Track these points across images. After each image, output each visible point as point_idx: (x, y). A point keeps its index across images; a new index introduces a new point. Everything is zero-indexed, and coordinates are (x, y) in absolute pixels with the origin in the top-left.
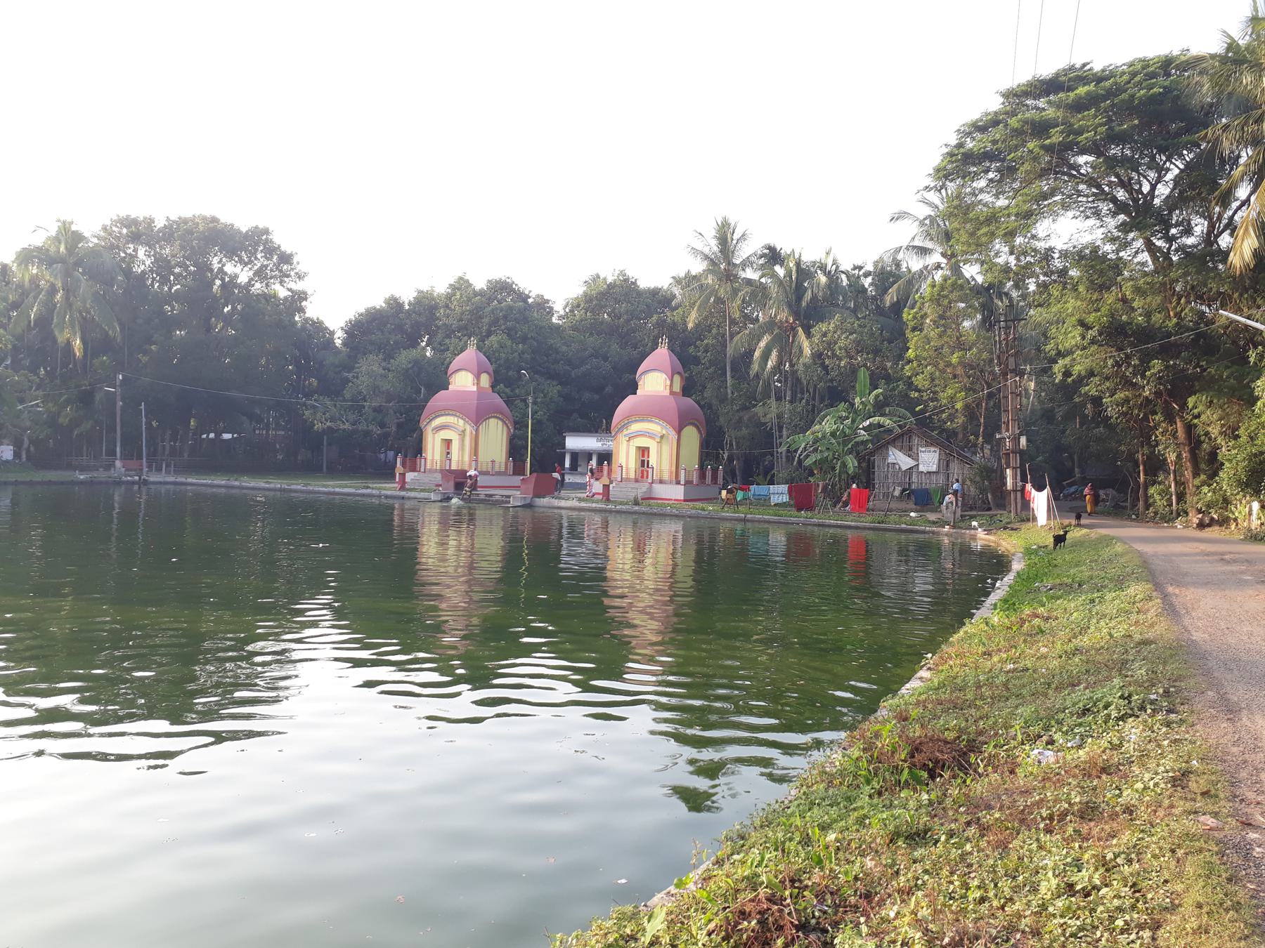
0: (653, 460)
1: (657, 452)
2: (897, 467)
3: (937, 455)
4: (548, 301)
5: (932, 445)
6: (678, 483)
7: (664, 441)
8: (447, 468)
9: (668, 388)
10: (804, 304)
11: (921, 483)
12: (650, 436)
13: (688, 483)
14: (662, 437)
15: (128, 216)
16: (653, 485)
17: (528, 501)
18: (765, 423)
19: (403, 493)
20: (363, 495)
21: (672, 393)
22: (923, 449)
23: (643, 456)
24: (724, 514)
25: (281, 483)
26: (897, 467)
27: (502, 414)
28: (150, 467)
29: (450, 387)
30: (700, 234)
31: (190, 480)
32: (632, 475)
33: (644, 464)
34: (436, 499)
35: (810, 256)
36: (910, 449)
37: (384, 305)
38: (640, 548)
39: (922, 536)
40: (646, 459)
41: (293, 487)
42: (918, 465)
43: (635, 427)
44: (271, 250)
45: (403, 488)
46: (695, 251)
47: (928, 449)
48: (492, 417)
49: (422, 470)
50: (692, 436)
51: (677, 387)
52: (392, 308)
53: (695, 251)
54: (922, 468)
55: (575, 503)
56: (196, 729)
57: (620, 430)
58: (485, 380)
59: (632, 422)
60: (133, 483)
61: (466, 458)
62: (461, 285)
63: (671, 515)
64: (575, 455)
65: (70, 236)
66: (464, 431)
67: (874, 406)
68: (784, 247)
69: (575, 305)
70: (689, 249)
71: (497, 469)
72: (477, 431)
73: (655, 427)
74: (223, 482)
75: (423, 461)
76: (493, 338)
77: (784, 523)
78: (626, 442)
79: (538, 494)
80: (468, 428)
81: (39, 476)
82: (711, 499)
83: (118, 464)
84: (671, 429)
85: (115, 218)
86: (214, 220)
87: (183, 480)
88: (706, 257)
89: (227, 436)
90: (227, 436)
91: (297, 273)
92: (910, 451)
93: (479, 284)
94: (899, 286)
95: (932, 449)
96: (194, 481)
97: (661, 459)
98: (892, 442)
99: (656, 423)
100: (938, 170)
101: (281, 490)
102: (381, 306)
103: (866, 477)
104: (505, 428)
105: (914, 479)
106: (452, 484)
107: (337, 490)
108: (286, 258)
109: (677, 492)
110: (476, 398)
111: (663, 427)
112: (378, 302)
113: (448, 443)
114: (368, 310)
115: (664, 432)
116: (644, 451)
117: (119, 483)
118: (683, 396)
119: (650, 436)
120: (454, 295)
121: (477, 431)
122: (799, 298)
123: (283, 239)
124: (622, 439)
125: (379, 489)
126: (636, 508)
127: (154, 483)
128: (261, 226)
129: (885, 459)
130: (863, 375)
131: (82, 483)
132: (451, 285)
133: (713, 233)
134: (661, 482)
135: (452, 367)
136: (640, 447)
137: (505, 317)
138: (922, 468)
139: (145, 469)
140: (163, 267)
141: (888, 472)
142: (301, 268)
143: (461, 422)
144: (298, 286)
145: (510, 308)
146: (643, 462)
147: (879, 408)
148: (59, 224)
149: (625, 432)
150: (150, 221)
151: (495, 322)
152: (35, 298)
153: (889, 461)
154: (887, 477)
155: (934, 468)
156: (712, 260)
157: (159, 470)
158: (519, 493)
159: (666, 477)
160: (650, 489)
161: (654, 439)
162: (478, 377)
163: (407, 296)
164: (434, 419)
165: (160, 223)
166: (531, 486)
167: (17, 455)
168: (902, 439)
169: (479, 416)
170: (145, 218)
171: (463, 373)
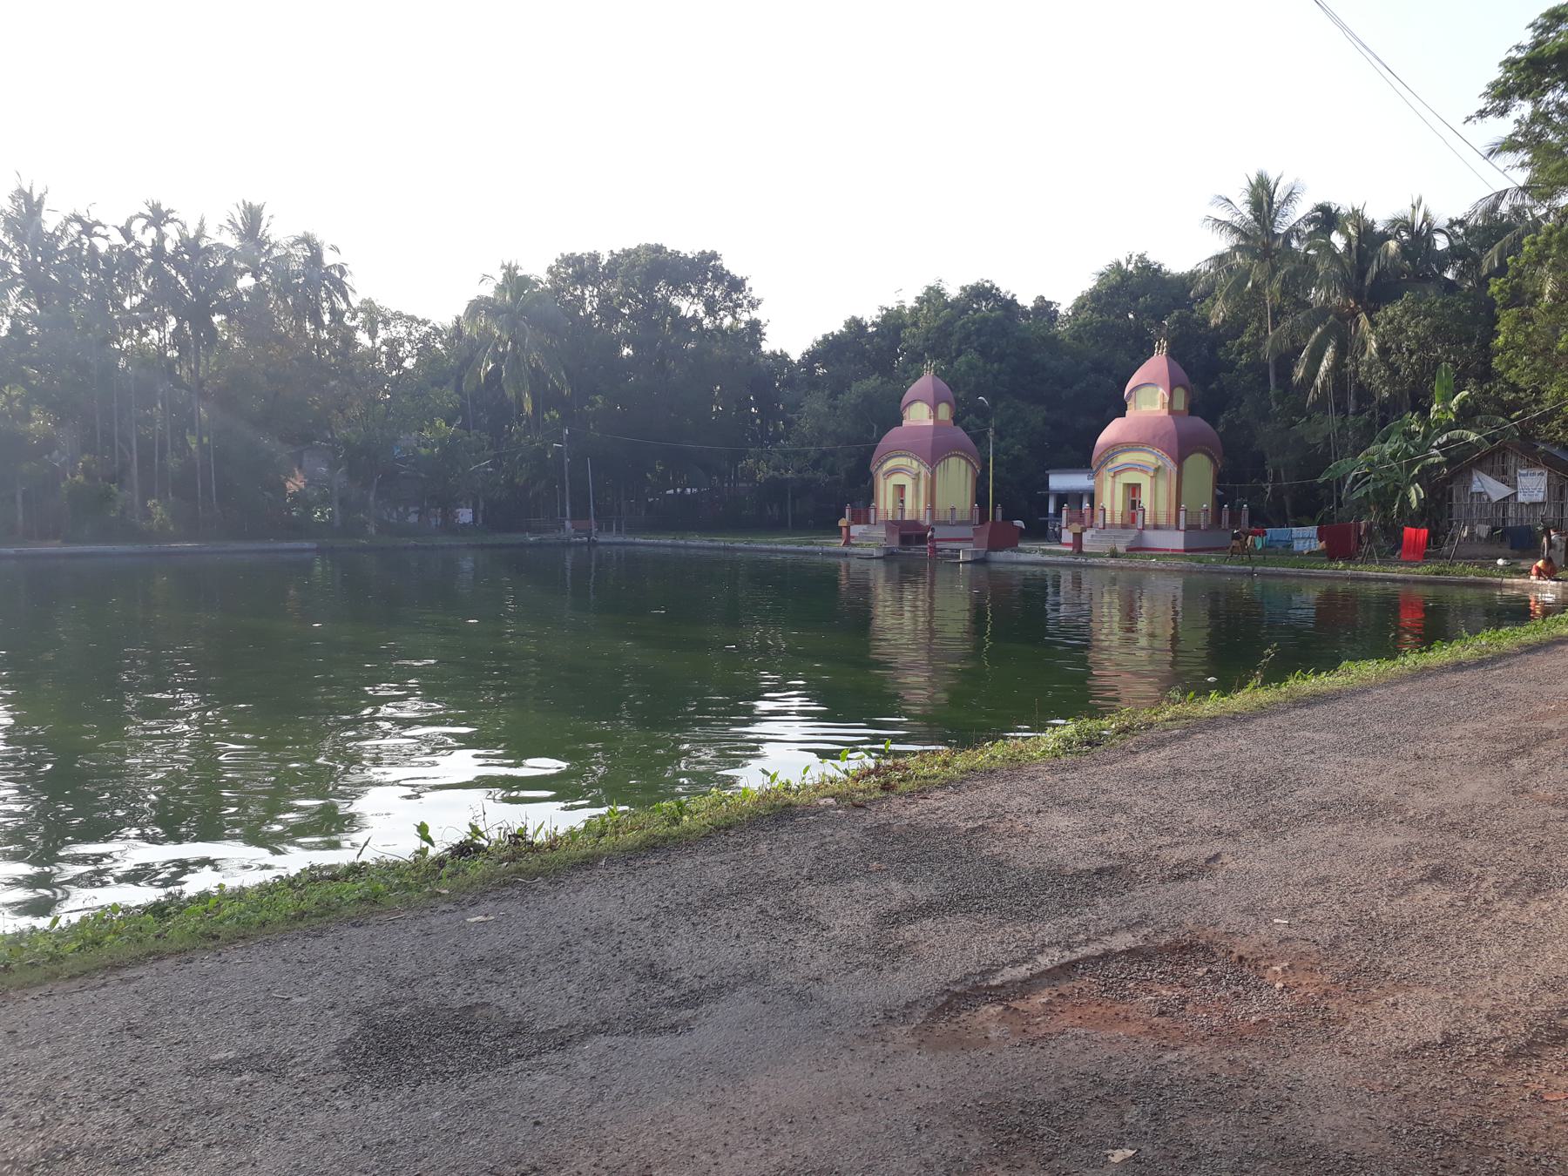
0: (1145, 499)
1: (1151, 489)
2: (1486, 497)
3: (1544, 479)
4: (1051, 303)
5: (1537, 465)
6: (1178, 528)
7: (1159, 475)
8: (899, 518)
9: (1166, 406)
10: (1368, 282)
11: (1521, 519)
12: (1142, 468)
13: (1188, 528)
14: (1157, 470)
15: (573, 254)
16: (1145, 532)
17: (981, 555)
18: (1314, 445)
19: (1081, 560)
20: (806, 553)
21: (1171, 412)
22: (1524, 472)
23: (1134, 495)
24: (1224, 567)
25: (725, 541)
26: (1486, 497)
27: (965, 451)
28: (600, 529)
29: (904, 422)
30: (1228, 200)
31: (637, 540)
32: (1118, 520)
33: (1134, 505)
34: (879, 555)
35: (1379, 215)
36: (1505, 472)
37: (844, 330)
38: (1130, 615)
39: (632, 548)
40: (1137, 498)
41: (737, 545)
42: (1515, 494)
43: (1123, 459)
44: (721, 276)
45: (847, 543)
46: (1220, 224)
47: (1531, 471)
48: (952, 456)
49: (873, 522)
50: (1201, 468)
51: (1180, 404)
52: (852, 333)
53: (1220, 224)
54: (1521, 498)
55: (1038, 557)
56: (519, 775)
57: (1104, 463)
58: (944, 412)
59: (1117, 453)
60: (582, 544)
61: (922, 507)
62: (933, 296)
63: (1156, 570)
64: (1063, 498)
65: (514, 282)
66: (918, 475)
67: (1457, 415)
68: (1343, 202)
69: (1080, 306)
70: (1211, 223)
71: (958, 518)
72: (933, 474)
73: (1148, 458)
74: (669, 541)
75: (872, 511)
76: (962, 359)
77: (1306, 577)
78: (1110, 479)
79: (995, 545)
80: (923, 470)
81: (499, 538)
82: (1221, 548)
83: (568, 524)
84: (1169, 459)
85: (560, 258)
86: (659, 249)
87: (631, 540)
88: (1235, 230)
89: (671, 492)
90: (671, 492)
91: (749, 302)
92: (1504, 476)
93: (953, 292)
94: (1502, 246)
95: (1538, 471)
96: (642, 541)
97: (1156, 499)
98: (1480, 464)
99: (1150, 452)
100: (1494, 86)
101: (726, 549)
102: (841, 331)
103: (1437, 514)
104: (970, 468)
105: (1511, 512)
106: (897, 537)
107: (779, 547)
108: (737, 285)
109: (1176, 540)
110: (931, 433)
111: (1158, 457)
112: (837, 326)
113: (901, 489)
114: (825, 337)
115: (1160, 463)
116: (1134, 489)
117: (569, 545)
118: (1189, 415)
119: (1142, 468)
120: (921, 309)
121: (933, 474)
122: (1362, 274)
123: (733, 265)
124: (1106, 475)
125: (821, 545)
126: (1113, 561)
127: (603, 544)
128: (708, 251)
129: (1467, 487)
130: (1446, 371)
131: (531, 545)
132: (918, 298)
133: (1246, 197)
134: (1156, 527)
135: (906, 398)
136: (1129, 484)
137: (978, 331)
138: (1521, 498)
139: (594, 530)
140: (608, 309)
141: (1472, 504)
142: (755, 294)
143: (915, 464)
144: (755, 314)
145: (985, 320)
146: (1134, 503)
147: (1467, 415)
148: (504, 271)
149: (1110, 466)
150: (595, 258)
151: (967, 337)
152: (485, 351)
153: (1474, 490)
154: (1470, 512)
155: (1540, 497)
156: (1242, 232)
157: (609, 529)
158: (972, 545)
159: (1162, 520)
160: (1140, 536)
161: (1146, 472)
162: (934, 408)
163: (870, 314)
164: (885, 461)
165: (605, 259)
166: (986, 537)
167: (475, 519)
168: (1494, 459)
169: (935, 452)
170: (590, 254)
171: (918, 405)
